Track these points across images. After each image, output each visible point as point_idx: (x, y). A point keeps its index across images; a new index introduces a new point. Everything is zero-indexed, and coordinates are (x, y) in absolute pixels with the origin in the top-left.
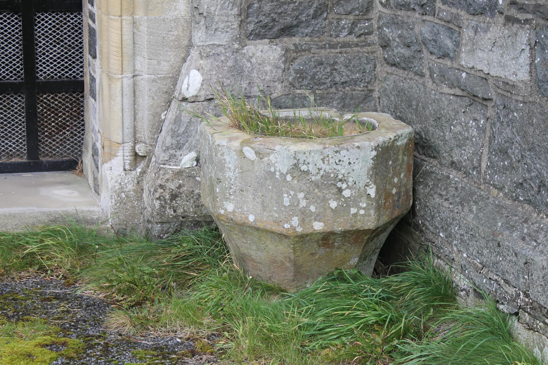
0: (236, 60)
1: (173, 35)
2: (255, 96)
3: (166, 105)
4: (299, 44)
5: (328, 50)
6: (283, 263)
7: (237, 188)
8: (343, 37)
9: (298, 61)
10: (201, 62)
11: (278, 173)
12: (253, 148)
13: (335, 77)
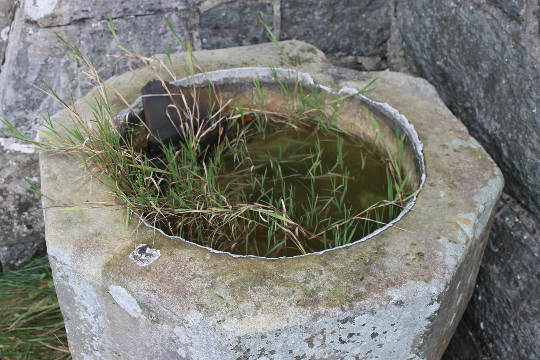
2: (169, 10)
3: (6, 16)
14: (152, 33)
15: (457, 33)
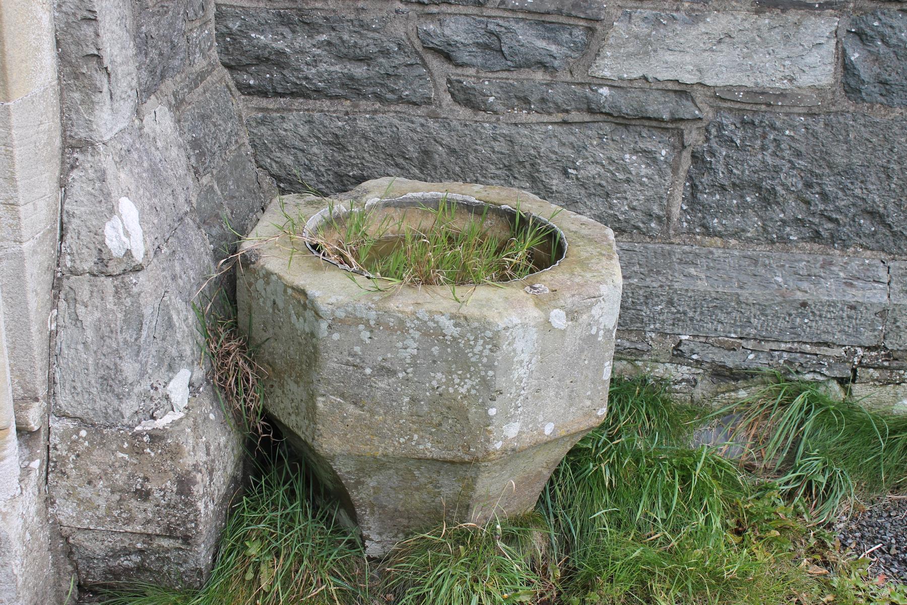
12: (562, 308)
15: (363, 140)
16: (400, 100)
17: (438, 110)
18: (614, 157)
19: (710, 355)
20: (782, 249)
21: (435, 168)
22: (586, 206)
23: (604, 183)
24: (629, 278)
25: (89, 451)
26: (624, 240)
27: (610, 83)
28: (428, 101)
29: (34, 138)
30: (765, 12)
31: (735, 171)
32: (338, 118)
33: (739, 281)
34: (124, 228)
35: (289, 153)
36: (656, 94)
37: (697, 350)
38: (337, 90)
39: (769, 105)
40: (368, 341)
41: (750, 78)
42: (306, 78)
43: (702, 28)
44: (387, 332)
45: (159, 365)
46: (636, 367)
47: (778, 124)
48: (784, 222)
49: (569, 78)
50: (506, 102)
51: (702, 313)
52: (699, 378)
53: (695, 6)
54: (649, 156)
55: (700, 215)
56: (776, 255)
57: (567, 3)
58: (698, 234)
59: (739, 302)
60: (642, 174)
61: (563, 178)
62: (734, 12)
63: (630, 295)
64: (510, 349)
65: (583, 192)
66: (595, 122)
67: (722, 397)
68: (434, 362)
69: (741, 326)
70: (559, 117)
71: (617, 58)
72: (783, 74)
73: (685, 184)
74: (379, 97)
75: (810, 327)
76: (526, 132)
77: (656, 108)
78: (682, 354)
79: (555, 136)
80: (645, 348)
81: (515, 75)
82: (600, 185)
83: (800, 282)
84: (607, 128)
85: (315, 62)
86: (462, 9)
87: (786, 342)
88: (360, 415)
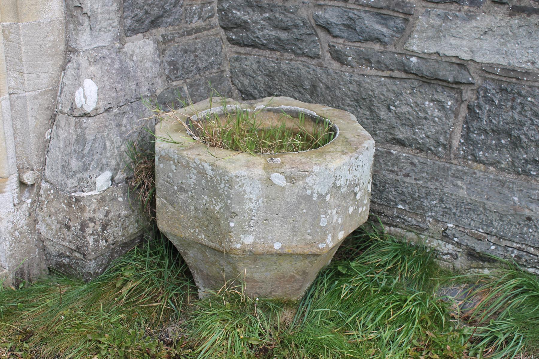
0: (121, 61)
1: (50, 41)
4: (166, 34)
5: (187, 38)
6: (292, 277)
7: (260, 219)
8: (196, 23)
9: (167, 53)
10: (91, 69)
11: (315, 195)
12: (282, 173)
13: (198, 64)
14: (140, 110)
15: (283, 76)
16: (304, 54)
17: (323, 62)
18: (419, 103)
19: (466, 241)
20: (525, 179)
21: (318, 96)
22: (400, 131)
23: (411, 118)
24: (418, 180)
25: (52, 201)
26: (422, 156)
27: (417, 55)
28: (317, 56)
29: (40, 43)
30: (515, 15)
31: (494, 121)
32: (273, 61)
33: (487, 195)
34: (84, 94)
35: (247, 78)
36: (445, 64)
37: (457, 235)
38: (273, 46)
39: (518, 79)
40: (175, 171)
41: (505, 59)
42: (257, 37)
43: (474, 23)
44: (183, 168)
45: (97, 167)
46: (420, 238)
47: (523, 92)
48: (527, 161)
49: (393, 50)
50: (358, 61)
51: (461, 211)
52: (459, 255)
53: (471, 9)
54: (441, 105)
55: (471, 147)
56: (519, 182)
57: (393, 2)
58: (470, 160)
59: (485, 209)
60: (435, 115)
61: (387, 111)
62: (495, 14)
63: (417, 191)
64: (241, 189)
65: (399, 122)
66: (409, 79)
67: (473, 271)
68: (203, 189)
69: (486, 225)
70: (388, 73)
71: (421, 39)
72: (527, 59)
73: (463, 126)
74: (294, 52)
75: (534, 236)
76: (368, 81)
77: (444, 73)
78: (447, 236)
79: (385, 85)
80: (425, 227)
81: (364, 45)
82: (409, 119)
83: (530, 203)
84: (416, 83)
85: (262, 29)
86: (336, 3)
87: (517, 243)
88: (174, 212)
